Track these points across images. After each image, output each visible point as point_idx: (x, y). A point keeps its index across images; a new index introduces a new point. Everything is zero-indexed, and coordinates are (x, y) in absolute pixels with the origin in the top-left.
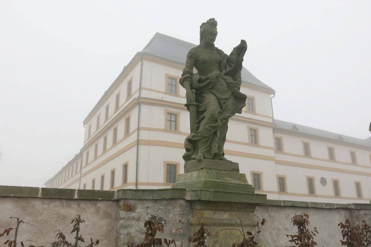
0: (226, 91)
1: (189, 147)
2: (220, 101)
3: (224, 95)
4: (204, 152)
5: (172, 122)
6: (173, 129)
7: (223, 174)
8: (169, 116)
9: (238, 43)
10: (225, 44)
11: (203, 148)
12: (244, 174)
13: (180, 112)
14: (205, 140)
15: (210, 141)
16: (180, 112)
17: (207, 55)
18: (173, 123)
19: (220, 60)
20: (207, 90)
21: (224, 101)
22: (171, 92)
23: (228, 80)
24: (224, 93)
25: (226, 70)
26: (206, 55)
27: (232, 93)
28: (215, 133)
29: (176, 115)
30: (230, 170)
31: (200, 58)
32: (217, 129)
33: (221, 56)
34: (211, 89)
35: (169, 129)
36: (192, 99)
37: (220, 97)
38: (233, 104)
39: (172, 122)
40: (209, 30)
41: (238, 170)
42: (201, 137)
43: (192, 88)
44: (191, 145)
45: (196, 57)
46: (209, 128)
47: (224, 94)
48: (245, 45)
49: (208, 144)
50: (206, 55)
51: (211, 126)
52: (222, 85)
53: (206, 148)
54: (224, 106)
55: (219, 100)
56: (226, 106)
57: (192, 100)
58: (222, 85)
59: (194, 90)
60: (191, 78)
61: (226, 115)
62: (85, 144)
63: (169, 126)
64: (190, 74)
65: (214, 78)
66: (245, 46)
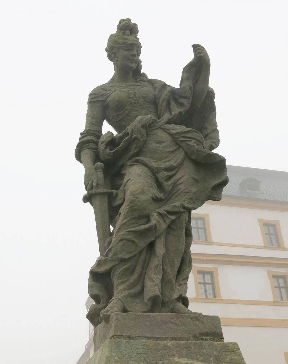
0: (172, 152)
1: (96, 292)
2: (157, 175)
3: (166, 162)
4: (127, 297)
5: (207, 286)
6: (210, 296)
7: (166, 347)
8: (201, 276)
9: (190, 57)
10: (163, 65)
11: (122, 287)
12: (235, 344)
13: (217, 268)
14: (125, 267)
15: (138, 269)
16: (217, 268)
17: (123, 90)
18: (209, 287)
19: (154, 95)
20: (129, 159)
21: (164, 172)
22: (199, 239)
23: (173, 129)
24: (167, 157)
25: (171, 114)
26: (120, 91)
27: (186, 153)
28: (151, 246)
29: (211, 273)
30: (195, 337)
31: (109, 99)
32: (153, 239)
33: (155, 89)
34: (138, 154)
35: (204, 297)
36: (95, 181)
37: (156, 166)
38: (194, 178)
39: (207, 286)
40: (124, 45)
41: (219, 336)
42: (115, 260)
43: (97, 158)
44: (100, 285)
45: (102, 101)
46: (130, 237)
47: (167, 159)
48: (201, 53)
49: (135, 277)
50: (120, 91)
51: (135, 232)
52: (160, 142)
53: (131, 286)
54: (168, 185)
55: (154, 172)
56: (175, 185)
57: (94, 184)
58: (160, 142)
59: (99, 164)
60: (97, 143)
61: (175, 204)
62: (90, 337)
63: (203, 291)
64: (93, 134)
65: (138, 128)
66: (202, 54)
